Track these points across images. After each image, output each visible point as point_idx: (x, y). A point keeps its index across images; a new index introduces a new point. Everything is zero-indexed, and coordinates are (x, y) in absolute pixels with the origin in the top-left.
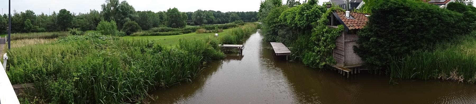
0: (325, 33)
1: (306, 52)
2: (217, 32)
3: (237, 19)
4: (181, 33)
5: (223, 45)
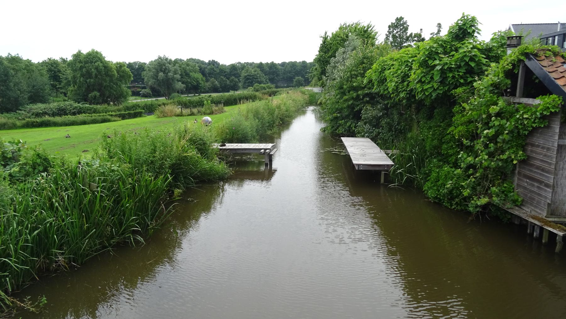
0: (493, 118)
1: (434, 166)
2: (211, 113)
3: (258, 81)
4: (113, 118)
5: (225, 145)
